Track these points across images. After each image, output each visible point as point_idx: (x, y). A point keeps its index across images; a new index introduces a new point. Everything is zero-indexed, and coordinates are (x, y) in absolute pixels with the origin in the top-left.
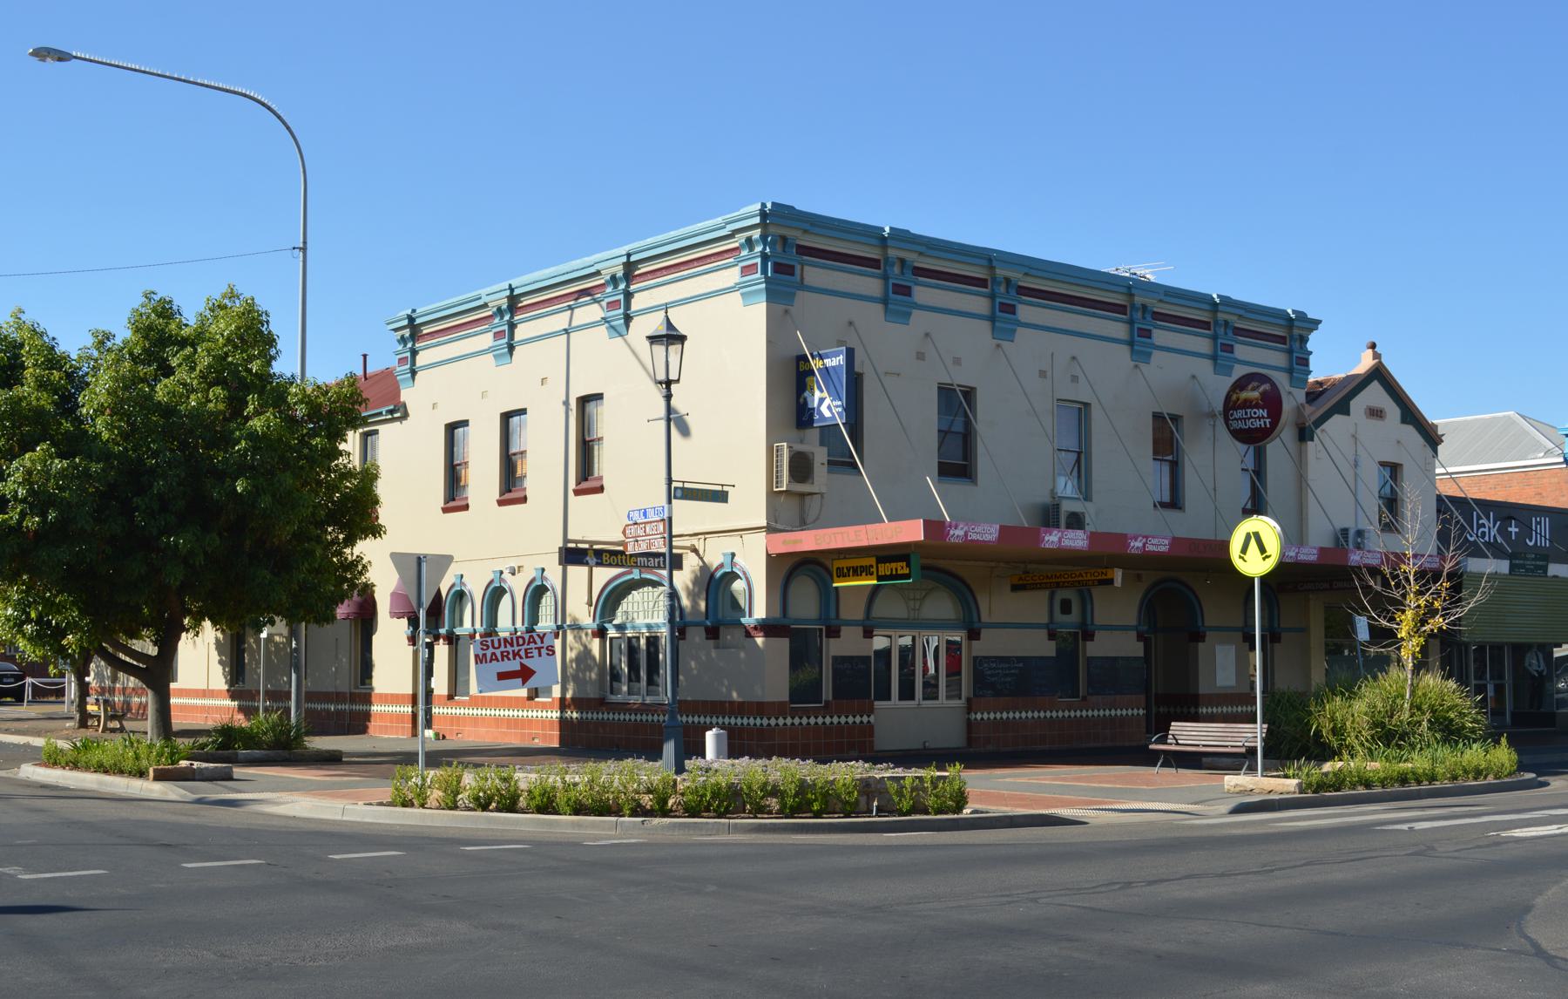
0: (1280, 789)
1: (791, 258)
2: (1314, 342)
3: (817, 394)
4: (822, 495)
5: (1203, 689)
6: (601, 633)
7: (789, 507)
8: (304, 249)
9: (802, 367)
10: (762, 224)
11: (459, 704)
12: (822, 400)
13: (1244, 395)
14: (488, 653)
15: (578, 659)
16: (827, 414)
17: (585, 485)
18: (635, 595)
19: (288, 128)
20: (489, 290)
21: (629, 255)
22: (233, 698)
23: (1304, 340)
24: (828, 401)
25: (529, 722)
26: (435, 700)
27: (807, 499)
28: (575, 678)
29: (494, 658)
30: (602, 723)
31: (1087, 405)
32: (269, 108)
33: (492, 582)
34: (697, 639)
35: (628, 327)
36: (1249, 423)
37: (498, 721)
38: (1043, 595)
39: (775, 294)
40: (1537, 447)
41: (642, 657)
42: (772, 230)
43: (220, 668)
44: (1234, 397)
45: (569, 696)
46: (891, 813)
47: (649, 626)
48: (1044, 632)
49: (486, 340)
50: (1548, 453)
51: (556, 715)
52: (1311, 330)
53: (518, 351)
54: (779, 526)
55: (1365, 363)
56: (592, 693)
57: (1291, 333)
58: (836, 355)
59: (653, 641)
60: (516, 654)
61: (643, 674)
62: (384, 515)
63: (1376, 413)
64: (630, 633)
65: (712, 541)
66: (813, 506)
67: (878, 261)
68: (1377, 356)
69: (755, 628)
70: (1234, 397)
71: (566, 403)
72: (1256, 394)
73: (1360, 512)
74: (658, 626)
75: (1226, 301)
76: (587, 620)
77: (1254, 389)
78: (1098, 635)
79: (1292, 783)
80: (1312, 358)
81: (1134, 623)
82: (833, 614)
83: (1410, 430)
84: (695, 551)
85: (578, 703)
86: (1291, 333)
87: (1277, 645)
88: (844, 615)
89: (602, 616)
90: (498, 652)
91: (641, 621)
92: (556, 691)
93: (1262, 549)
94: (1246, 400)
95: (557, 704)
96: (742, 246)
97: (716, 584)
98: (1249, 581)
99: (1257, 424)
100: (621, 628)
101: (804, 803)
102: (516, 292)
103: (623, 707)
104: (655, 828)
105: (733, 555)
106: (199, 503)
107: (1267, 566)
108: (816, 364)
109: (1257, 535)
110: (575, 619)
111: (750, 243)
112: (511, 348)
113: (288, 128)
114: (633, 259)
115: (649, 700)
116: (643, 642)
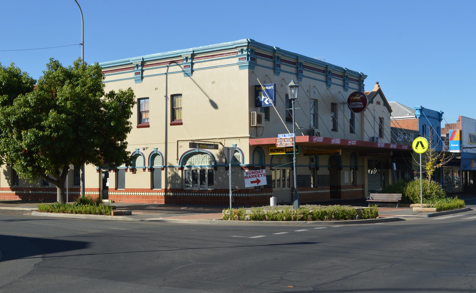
0: (431, 211)
1: (254, 56)
2: (366, 82)
3: (263, 97)
4: (263, 127)
5: (342, 184)
6: (182, 168)
7: (255, 132)
8: (83, 44)
9: (257, 88)
10: (248, 46)
11: (155, 191)
12: (265, 99)
13: (355, 98)
14: (248, 176)
15: (172, 177)
16: (267, 103)
17: (173, 122)
18: (194, 157)
19: (78, 4)
20: (134, 58)
21: (194, 51)
22: (13, 190)
23: (363, 81)
24: (267, 100)
25: (152, 196)
26: (86, 190)
27: (259, 128)
28: (171, 183)
33: (153, 152)
34: (222, 171)
35: (192, 74)
36: (357, 107)
38: (308, 157)
39: (251, 67)
41: (199, 176)
42: (250, 47)
43: (6, 181)
44: (352, 98)
45: (169, 188)
46: (362, 218)
47: (201, 167)
49: (132, 75)
50: (410, 114)
51: (163, 194)
52: (365, 78)
55: (376, 89)
56: (177, 187)
57: (360, 79)
58: (271, 86)
59: (203, 171)
60: (255, 176)
61: (199, 181)
63: (378, 103)
64: (193, 168)
65: (227, 141)
68: (379, 86)
69: (245, 167)
70: (352, 98)
71: (166, 96)
72: (359, 98)
74: (205, 166)
75: (348, 70)
76: (176, 164)
77: (358, 96)
78: (320, 169)
80: (365, 87)
81: (327, 165)
82: (264, 163)
83: (385, 108)
84: (221, 144)
85: (171, 190)
86: (360, 79)
88: (266, 163)
89: (182, 165)
93: (423, 146)
94: (356, 100)
95: (164, 191)
96: (239, 51)
98: (418, 155)
99: (359, 107)
100: (189, 167)
101: (337, 217)
103: (191, 191)
104: (309, 224)
105: (236, 145)
106: (78, 127)
107: (424, 150)
108: (263, 88)
109: (421, 142)
110: (171, 164)
111: (242, 51)
112: (142, 78)
113: (78, 4)
114: (195, 53)
115: (201, 189)
116: (198, 171)
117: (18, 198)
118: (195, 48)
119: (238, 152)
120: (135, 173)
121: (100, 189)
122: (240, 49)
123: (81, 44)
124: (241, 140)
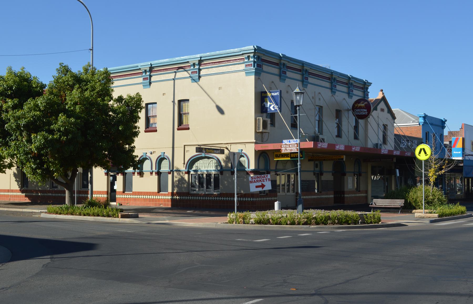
0: (433, 217)
1: (260, 63)
3: (269, 103)
6: (188, 173)
7: (260, 137)
8: (92, 50)
9: (263, 95)
10: (254, 53)
12: (270, 105)
14: (253, 180)
15: (179, 181)
16: (273, 109)
18: (201, 161)
20: (142, 64)
21: (201, 58)
23: (367, 88)
24: (273, 106)
25: (159, 200)
26: (94, 193)
28: (178, 186)
29: (255, 182)
30: (190, 200)
31: (322, 107)
32: (83, 4)
33: (160, 156)
34: (227, 175)
35: (199, 79)
36: (361, 113)
37: (145, 199)
39: (258, 73)
40: (410, 120)
41: (205, 180)
42: (257, 54)
43: (16, 183)
44: (356, 105)
45: (175, 191)
47: (207, 171)
48: (313, 173)
49: (140, 80)
50: (413, 122)
51: (170, 197)
52: (369, 86)
53: (152, 84)
54: (259, 142)
55: (380, 96)
56: (184, 191)
57: (364, 86)
58: (276, 92)
60: (260, 181)
61: (205, 185)
62: (138, 136)
63: (382, 110)
64: (199, 173)
65: (233, 146)
66: (266, 136)
67: (278, 64)
68: (383, 94)
69: (251, 172)
70: (356, 105)
71: (174, 102)
72: (363, 105)
73: (347, 135)
74: (211, 171)
76: (183, 168)
77: (362, 103)
78: (324, 174)
79: (436, 215)
80: (369, 94)
83: (389, 115)
84: (227, 149)
85: (178, 194)
86: (364, 86)
87: (361, 177)
88: (271, 168)
90: (256, 180)
91: (203, 169)
92: (170, 190)
93: (425, 153)
94: (360, 106)
95: (170, 194)
96: (246, 58)
97: (234, 158)
98: (421, 161)
99: (364, 113)
100: (196, 171)
102: (153, 66)
103: (197, 195)
104: (313, 228)
105: (242, 150)
106: (84, 132)
107: (427, 157)
108: (269, 95)
109: (424, 149)
110: (177, 168)
111: (249, 57)
112: (150, 83)
114: (202, 59)
115: (207, 193)
116: (205, 176)
117: (27, 200)
118: (202, 55)
119: (243, 156)
120: (142, 177)
121: (107, 192)
122: (246, 55)
123: (91, 50)
124: (247, 145)
